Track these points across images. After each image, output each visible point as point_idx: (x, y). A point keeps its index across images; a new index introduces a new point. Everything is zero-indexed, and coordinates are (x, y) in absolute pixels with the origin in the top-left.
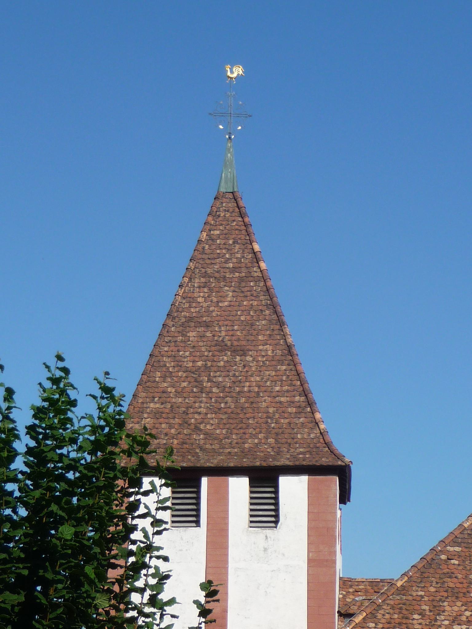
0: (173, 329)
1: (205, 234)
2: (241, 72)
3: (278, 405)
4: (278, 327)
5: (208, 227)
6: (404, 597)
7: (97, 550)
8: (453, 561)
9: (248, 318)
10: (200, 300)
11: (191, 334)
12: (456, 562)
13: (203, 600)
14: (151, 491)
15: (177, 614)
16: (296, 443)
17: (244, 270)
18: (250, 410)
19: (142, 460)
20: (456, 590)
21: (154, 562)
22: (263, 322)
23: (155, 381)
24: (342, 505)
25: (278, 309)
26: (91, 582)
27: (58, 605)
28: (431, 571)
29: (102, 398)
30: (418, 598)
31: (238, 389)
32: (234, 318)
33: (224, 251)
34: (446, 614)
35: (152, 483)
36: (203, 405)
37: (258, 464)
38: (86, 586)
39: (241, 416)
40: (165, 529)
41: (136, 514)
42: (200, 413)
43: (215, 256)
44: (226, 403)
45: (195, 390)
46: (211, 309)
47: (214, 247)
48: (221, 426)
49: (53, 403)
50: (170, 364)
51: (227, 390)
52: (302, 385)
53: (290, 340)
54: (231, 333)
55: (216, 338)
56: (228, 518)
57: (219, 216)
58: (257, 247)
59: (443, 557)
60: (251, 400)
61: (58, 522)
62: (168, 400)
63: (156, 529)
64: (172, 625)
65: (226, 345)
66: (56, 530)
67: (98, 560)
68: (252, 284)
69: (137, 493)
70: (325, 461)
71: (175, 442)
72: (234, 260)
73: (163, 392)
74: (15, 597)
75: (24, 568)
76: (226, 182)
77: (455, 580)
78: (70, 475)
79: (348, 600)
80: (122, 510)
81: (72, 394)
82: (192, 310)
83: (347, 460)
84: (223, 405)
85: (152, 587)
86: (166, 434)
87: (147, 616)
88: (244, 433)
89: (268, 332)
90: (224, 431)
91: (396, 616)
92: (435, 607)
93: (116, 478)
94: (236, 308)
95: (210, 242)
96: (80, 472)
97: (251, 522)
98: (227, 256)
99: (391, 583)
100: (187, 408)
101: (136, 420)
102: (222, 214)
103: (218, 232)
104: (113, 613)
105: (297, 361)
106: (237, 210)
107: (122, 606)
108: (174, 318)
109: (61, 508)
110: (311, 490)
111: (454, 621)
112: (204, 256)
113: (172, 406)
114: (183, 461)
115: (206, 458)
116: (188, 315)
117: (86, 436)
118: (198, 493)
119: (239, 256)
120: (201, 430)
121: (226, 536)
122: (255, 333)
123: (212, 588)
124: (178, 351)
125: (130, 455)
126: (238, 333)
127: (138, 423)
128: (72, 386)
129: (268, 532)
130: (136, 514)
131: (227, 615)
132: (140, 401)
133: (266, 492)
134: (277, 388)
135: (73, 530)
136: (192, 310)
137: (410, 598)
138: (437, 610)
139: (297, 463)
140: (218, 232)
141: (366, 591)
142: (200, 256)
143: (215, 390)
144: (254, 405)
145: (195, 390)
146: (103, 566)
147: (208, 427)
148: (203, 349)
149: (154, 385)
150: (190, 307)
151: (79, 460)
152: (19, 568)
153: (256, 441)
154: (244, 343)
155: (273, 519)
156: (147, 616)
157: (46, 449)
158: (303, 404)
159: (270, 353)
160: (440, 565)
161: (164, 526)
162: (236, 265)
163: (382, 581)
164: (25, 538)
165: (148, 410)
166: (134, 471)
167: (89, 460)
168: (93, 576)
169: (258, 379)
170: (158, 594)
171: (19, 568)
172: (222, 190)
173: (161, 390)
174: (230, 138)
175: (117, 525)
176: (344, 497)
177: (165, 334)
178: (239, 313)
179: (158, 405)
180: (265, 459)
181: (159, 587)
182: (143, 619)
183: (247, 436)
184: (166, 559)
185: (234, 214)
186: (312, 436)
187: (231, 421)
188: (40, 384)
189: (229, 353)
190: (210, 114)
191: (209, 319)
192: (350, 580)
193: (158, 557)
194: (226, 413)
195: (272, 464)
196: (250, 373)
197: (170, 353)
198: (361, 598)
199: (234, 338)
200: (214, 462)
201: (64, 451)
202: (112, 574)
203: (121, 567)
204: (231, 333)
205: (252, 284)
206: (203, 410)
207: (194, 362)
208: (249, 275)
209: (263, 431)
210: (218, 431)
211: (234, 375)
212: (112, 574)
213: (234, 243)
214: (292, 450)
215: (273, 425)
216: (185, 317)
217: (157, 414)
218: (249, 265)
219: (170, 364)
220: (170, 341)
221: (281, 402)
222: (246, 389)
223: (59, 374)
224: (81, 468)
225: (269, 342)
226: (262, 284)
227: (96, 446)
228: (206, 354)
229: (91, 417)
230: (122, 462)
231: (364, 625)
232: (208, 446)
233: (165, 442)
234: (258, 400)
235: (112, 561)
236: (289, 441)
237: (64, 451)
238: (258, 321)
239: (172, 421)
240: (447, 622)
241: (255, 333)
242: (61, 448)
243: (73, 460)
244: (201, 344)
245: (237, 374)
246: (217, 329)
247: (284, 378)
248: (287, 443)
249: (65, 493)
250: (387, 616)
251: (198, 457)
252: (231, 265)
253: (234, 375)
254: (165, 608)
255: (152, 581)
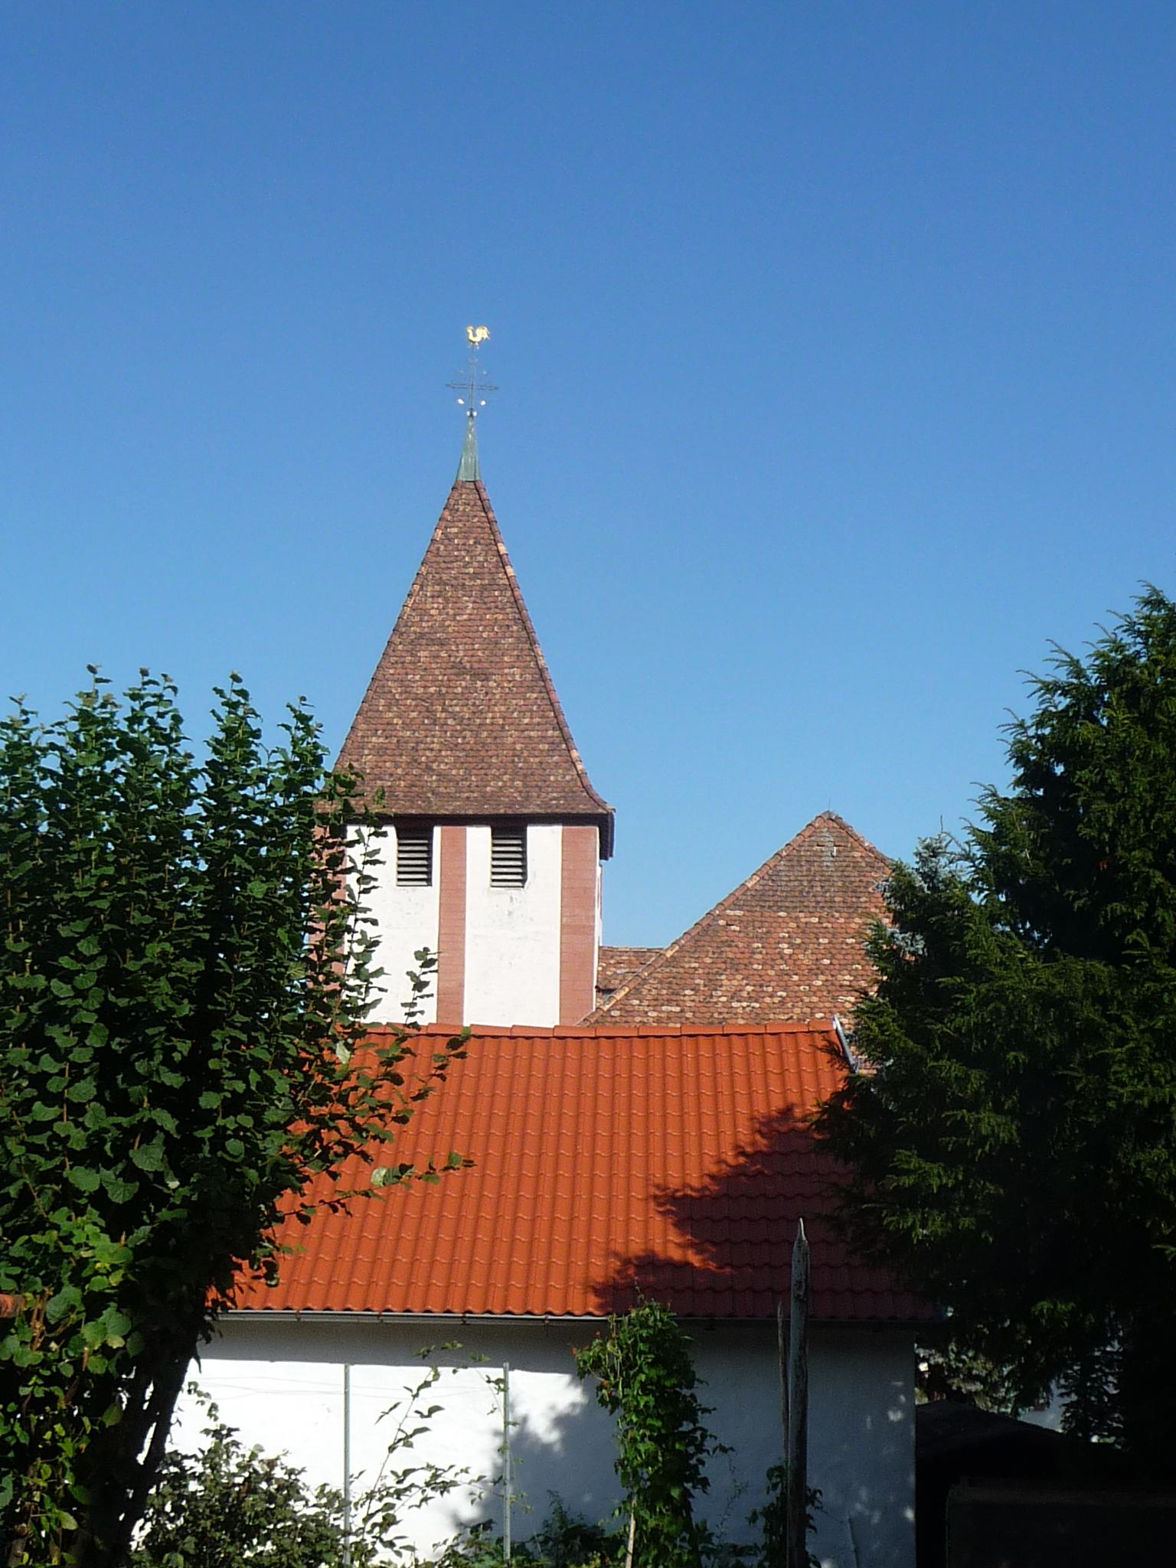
0: (400, 647)
1: (440, 532)
2: (486, 336)
3: (527, 741)
4: (528, 646)
5: (444, 524)
6: (675, 970)
7: (290, 910)
8: (733, 928)
9: (492, 634)
10: (433, 612)
11: (421, 654)
12: (738, 929)
13: (418, 971)
14: (358, 842)
15: (385, 987)
16: (548, 786)
17: (486, 576)
18: (494, 747)
19: (346, 804)
20: (736, 961)
21: (360, 926)
22: (510, 640)
23: (378, 711)
24: (603, 861)
25: (528, 624)
26: (284, 948)
27: (244, 975)
28: (708, 938)
29: (297, 728)
30: (691, 971)
31: (478, 721)
32: (475, 635)
33: (463, 553)
34: (724, 988)
35: (358, 832)
36: (436, 740)
37: (502, 811)
38: (279, 953)
39: (483, 753)
40: (374, 887)
41: (339, 869)
42: (432, 750)
43: (452, 559)
44: (464, 738)
45: (426, 721)
46: (447, 623)
47: (450, 548)
48: (458, 765)
49: (229, 731)
50: (397, 691)
51: (465, 722)
52: (556, 717)
53: (542, 662)
54: (470, 653)
55: (452, 659)
56: (464, 875)
57: (457, 510)
58: (502, 549)
59: (722, 922)
60: (495, 734)
61: (244, 879)
62: (394, 733)
63: (363, 887)
64: (380, 1000)
65: (465, 668)
66: (244, 887)
67: (291, 922)
68: (496, 593)
69: (341, 844)
70: (582, 808)
71: (403, 784)
72: (476, 564)
73: (388, 724)
74: (194, 964)
75: (205, 931)
76: (466, 469)
77: (735, 950)
78: (258, 821)
79: (609, 973)
80: (322, 865)
81: (253, 723)
82: (424, 624)
83: (609, 807)
84: (460, 740)
85: (357, 956)
86: (391, 775)
87: (352, 989)
88: (486, 775)
89: (516, 653)
90: (461, 772)
91: (664, 992)
92: (710, 980)
93: (312, 824)
94: (478, 623)
95: (446, 542)
96: (270, 817)
97: (493, 880)
98: (467, 559)
99: (660, 953)
100: (417, 743)
101: (356, 757)
102: (461, 508)
103: (456, 530)
104: (310, 985)
105: (550, 687)
106: (479, 503)
107: (321, 978)
108: (402, 634)
109: (247, 860)
110: (565, 841)
111: (732, 998)
112: (438, 559)
113: (398, 741)
114: (412, 808)
115: (439, 803)
116: (418, 630)
117: (277, 774)
118: (430, 845)
119: (481, 559)
120: (434, 770)
121: (463, 898)
122: (500, 653)
123: (429, 957)
124: (407, 674)
125: (331, 799)
126: (480, 653)
127: (357, 760)
128: (254, 713)
129: (513, 891)
130: (339, 869)
131: (463, 991)
132: (360, 734)
133: (511, 845)
134: (526, 721)
135: (265, 887)
136: (424, 624)
137: (681, 970)
138: (713, 984)
139: (549, 811)
140: (456, 530)
141: (630, 962)
142: (434, 559)
143: (450, 722)
144: (498, 741)
145: (426, 721)
146: (297, 930)
147: (442, 766)
148: (437, 672)
149: (377, 715)
150: (421, 620)
151: (268, 803)
152: (199, 931)
153: (500, 784)
154: (486, 665)
155: (519, 877)
156: (352, 989)
157: (226, 789)
158: (558, 740)
159: (517, 678)
160: (717, 932)
161: (373, 883)
162: (478, 570)
163: (649, 950)
164: (205, 895)
165: (370, 746)
166: (337, 817)
167: (280, 803)
168: (286, 942)
169: (503, 708)
170: (365, 963)
171: (199, 931)
172: (462, 478)
173: (386, 721)
174: (471, 415)
175: (315, 882)
176: (606, 852)
177: (391, 652)
178: (481, 629)
179: (381, 740)
180: (510, 806)
181: (366, 955)
182: (347, 992)
183: (489, 778)
184: (374, 922)
185: (475, 508)
186: (568, 778)
187: (470, 759)
188: (213, 712)
189: (468, 677)
190: (448, 385)
191: (445, 636)
192: (612, 949)
193: (365, 920)
194: (464, 750)
195: (518, 812)
196: (493, 702)
197: (396, 677)
198: (624, 971)
199: (474, 659)
200: (448, 809)
201: (249, 791)
202: (309, 940)
203: (321, 931)
204: (470, 653)
205: (496, 593)
206: (435, 746)
207: (425, 687)
208: (493, 583)
209: (510, 771)
210: (454, 772)
211: (474, 704)
212: (309, 940)
213: (475, 543)
214: (544, 795)
215: (520, 765)
216: (415, 633)
217: (380, 751)
218: (493, 570)
219: (397, 691)
220: (396, 662)
221: (530, 737)
222: (488, 721)
223: (235, 698)
224: (271, 812)
225: (516, 664)
226: (509, 593)
227: (290, 788)
228: (440, 678)
229: (283, 752)
230: (324, 806)
231: (627, 1002)
232: (442, 790)
233: (389, 784)
234: (504, 734)
235: (310, 924)
236: (540, 784)
237: (249, 791)
238: (504, 638)
239: (398, 759)
240: (724, 999)
241: (500, 653)
242: (244, 788)
243: (261, 802)
244: (434, 666)
245: (477, 702)
246: (453, 648)
247: (535, 708)
248: (537, 786)
249: (250, 842)
250: (654, 992)
251: (430, 802)
252: (471, 570)
253: (474, 704)
254: (371, 980)
255: (358, 949)
